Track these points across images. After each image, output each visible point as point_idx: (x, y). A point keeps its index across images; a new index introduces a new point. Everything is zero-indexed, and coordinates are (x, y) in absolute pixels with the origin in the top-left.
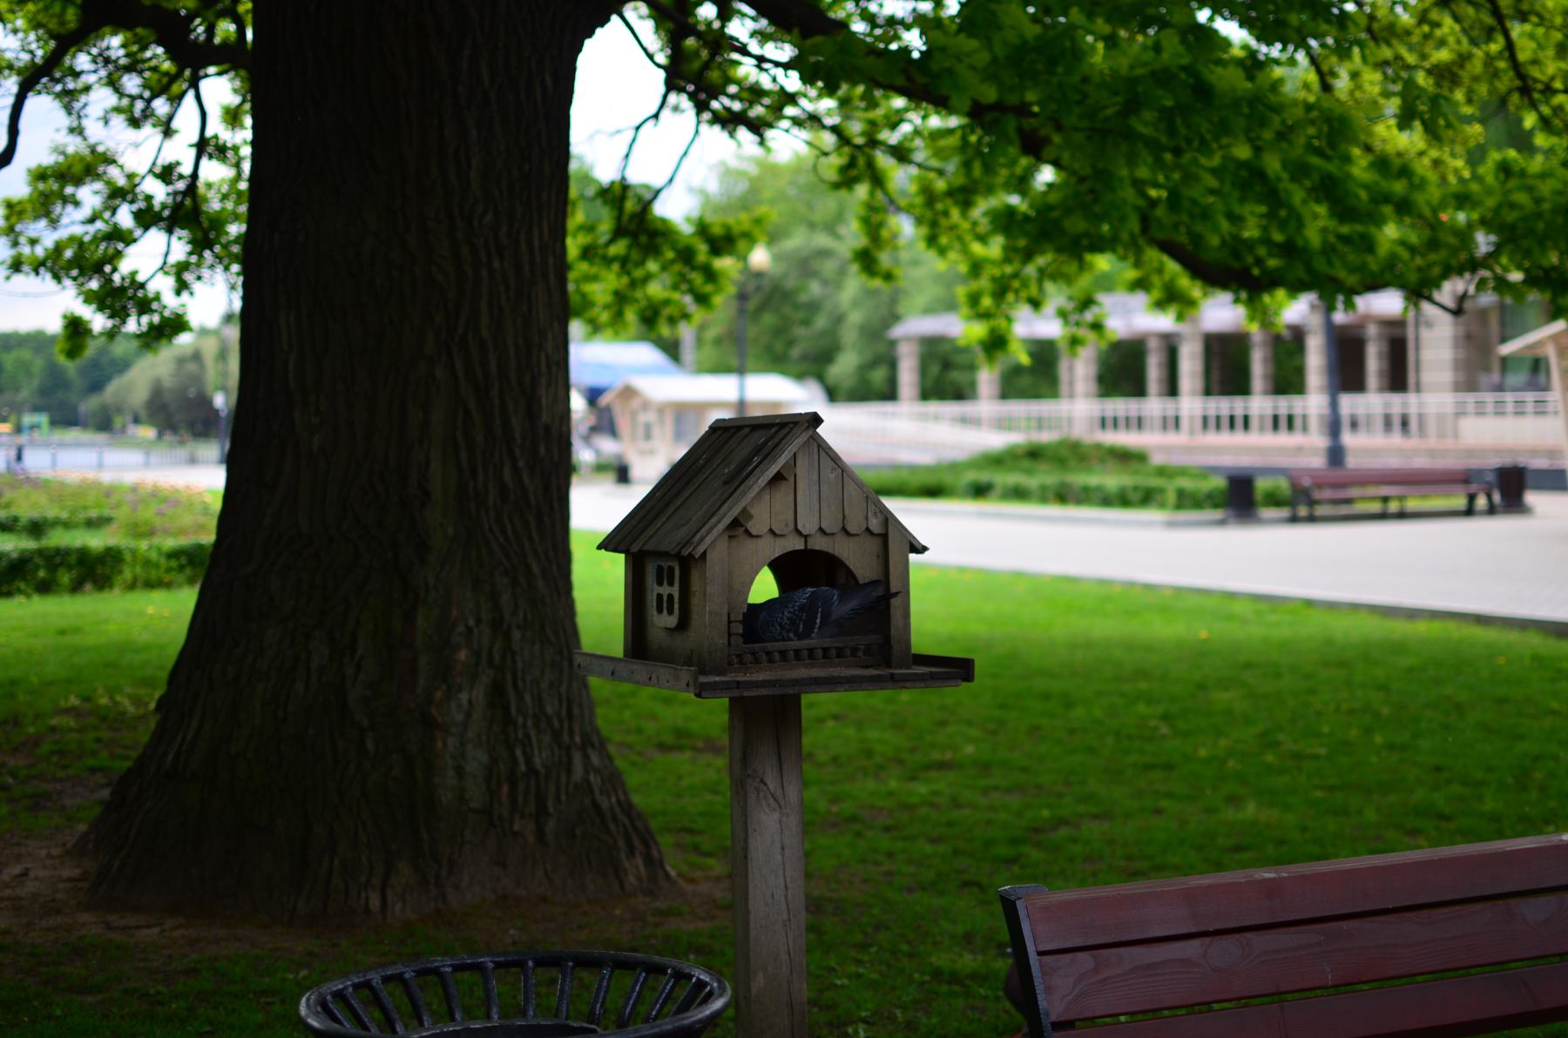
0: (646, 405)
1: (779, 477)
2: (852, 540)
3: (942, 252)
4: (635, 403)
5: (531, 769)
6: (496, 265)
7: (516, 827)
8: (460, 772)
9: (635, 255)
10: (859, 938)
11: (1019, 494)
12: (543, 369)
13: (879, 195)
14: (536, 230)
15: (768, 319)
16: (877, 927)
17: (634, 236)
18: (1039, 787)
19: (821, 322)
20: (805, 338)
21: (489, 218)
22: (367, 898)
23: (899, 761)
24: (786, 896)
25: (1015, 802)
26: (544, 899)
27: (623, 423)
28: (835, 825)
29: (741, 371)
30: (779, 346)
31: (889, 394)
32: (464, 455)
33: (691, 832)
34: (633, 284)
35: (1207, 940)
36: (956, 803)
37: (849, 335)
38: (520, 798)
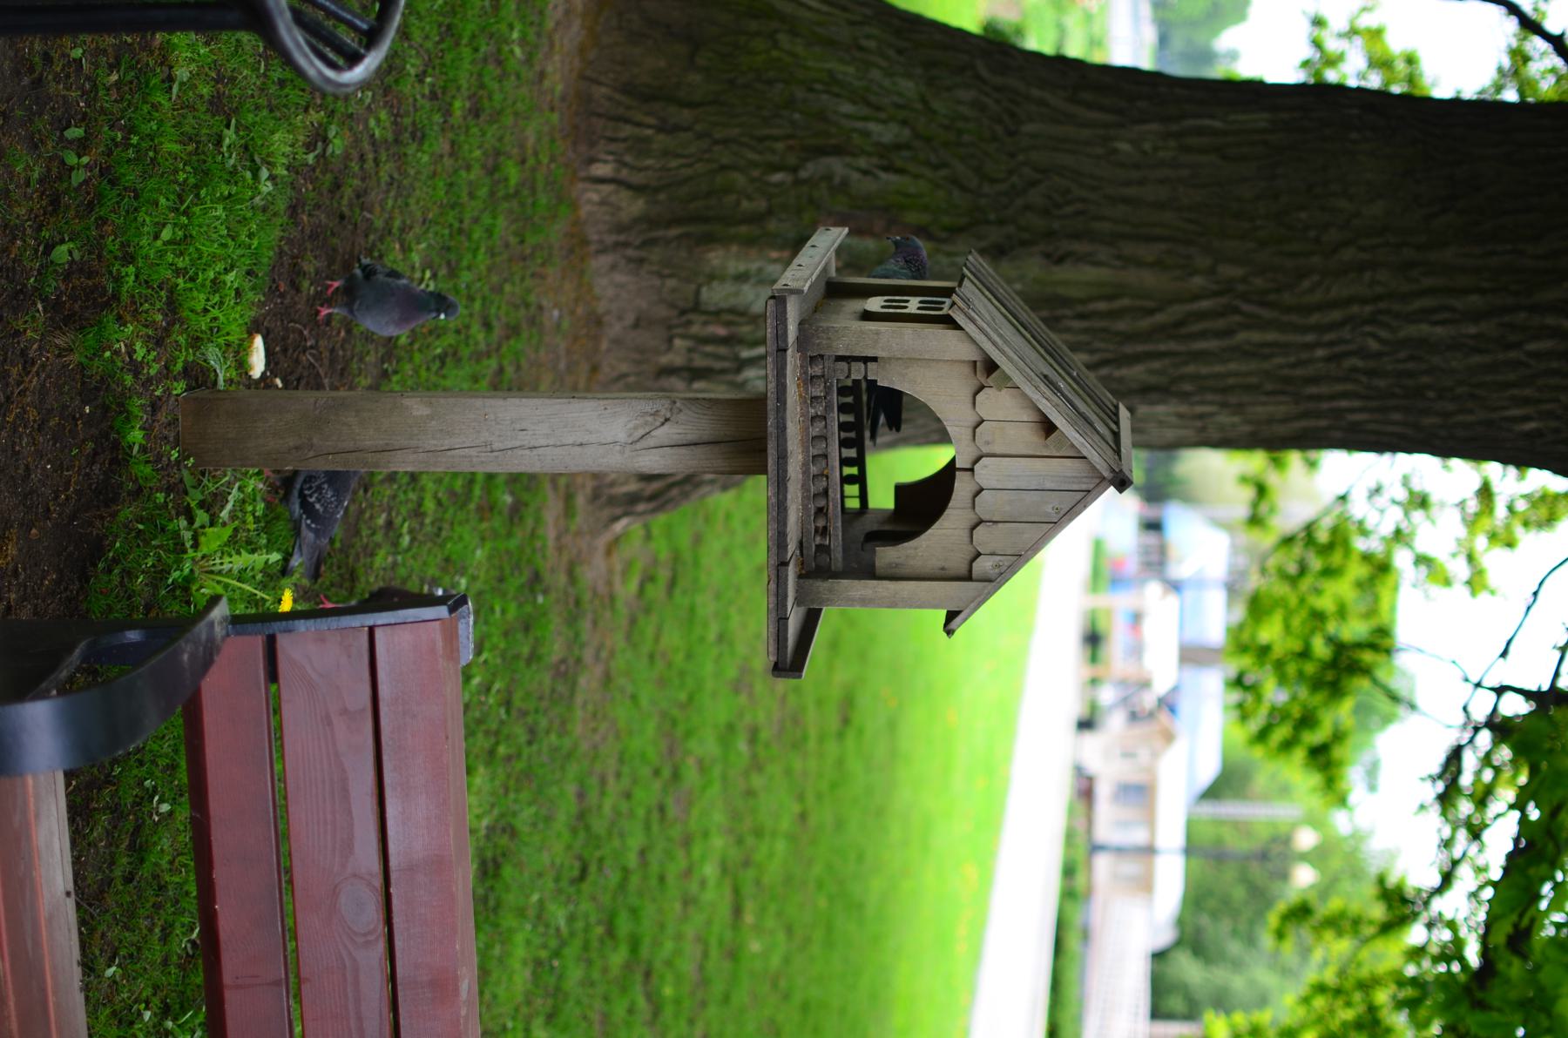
0: (1155, 755)
1: (1048, 428)
2: (966, 534)
3: (1306, 1000)
5: (743, 364)
6: (1320, 353)
7: (678, 342)
8: (742, 278)
9: (1310, 668)
10: (517, 702)
12: (1199, 409)
13: (1368, 931)
14: (1356, 404)
15: (1239, 893)
16: (532, 731)
17: (1333, 664)
18: (703, 1004)
19: (1235, 947)
20: (1218, 930)
21: (1373, 345)
22: (605, 162)
23: (747, 863)
24: (520, 447)
25: (687, 966)
26: (595, 369)
27: (1140, 730)
28: (671, 751)
29: (1190, 850)
30: (1212, 903)
32: (1102, 306)
33: (672, 584)
34: (1279, 666)
35: (378, 882)
36: (688, 902)
37: (1220, 975)
38: (709, 349)
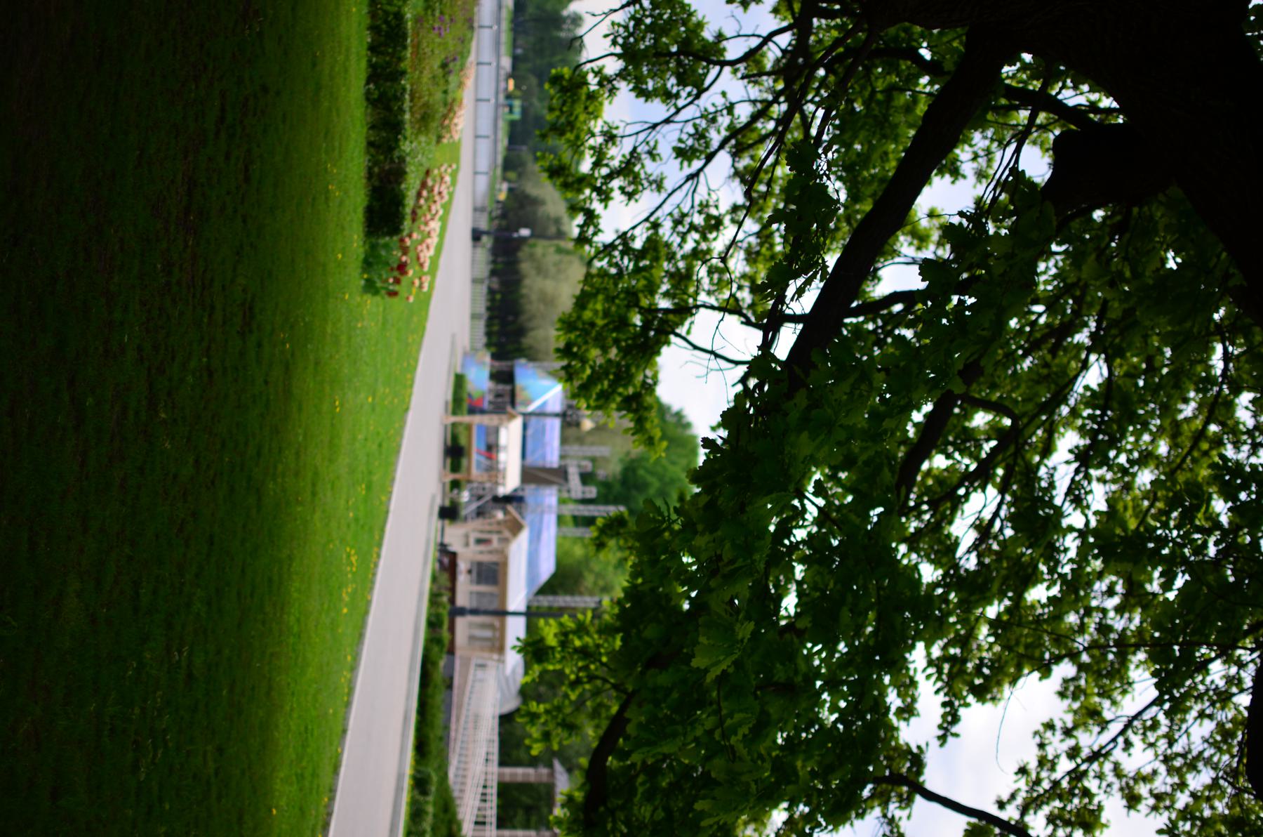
0: (506, 541)
4: (507, 534)
11: (416, 814)
31: (506, 758)
